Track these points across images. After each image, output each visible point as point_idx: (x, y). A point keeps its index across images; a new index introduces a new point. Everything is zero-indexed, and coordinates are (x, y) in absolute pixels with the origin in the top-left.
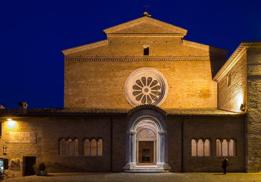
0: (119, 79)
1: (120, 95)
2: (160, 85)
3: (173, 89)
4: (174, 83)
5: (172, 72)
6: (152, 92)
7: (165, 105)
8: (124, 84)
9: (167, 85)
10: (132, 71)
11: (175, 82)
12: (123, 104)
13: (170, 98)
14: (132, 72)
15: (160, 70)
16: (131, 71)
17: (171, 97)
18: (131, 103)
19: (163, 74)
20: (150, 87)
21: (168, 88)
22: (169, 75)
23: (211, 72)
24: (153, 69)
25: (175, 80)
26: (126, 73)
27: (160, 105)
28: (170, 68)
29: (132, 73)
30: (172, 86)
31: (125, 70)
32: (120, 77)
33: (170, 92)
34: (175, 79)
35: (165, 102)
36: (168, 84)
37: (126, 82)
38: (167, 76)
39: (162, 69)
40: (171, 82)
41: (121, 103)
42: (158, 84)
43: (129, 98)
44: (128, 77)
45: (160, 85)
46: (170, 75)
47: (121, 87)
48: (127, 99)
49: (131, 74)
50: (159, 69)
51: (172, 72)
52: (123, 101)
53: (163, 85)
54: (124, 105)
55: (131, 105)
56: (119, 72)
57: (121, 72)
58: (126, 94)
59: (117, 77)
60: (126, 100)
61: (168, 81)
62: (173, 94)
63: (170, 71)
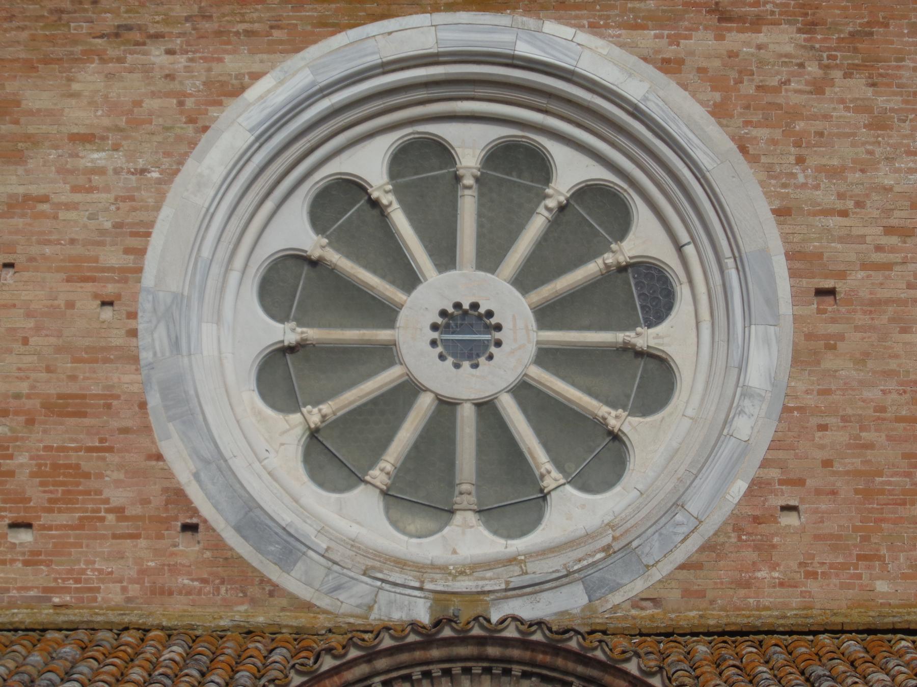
0: (63, 171)
1: (67, 407)
2: (599, 173)
3: (861, 318)
4: (874, 233)
5: (837, 74)
6: (547, 356)
7: (750, 555)
8: (141, 252)
9: (780, 266)
10: (256, 68)
11: (889, 230)
12: (106, 547)
13: (820, 455)
14: (256, 76)
15: (671, 52)
16: (233, 64)
17: (838, 437)
18: (238, 529)
19: (719, 112)
20: (410, 280)
21: (786, 308)
22: (800, 126)
23: (256, 389)
24: (567, 31)
25: (888, 189)
26: (168, 95)
27: (680, 556)
28: (810, 27)
29: (251, 94)
30: (855, 282)
31: (157, 55)
32: (87, 139)
33: (829, 362)
34: (885, 176)
35: (757, 520)
36: (789, 256)
37: (166, 212)
38: (777, 134)
39: (702, 44)
40: (820, 221)
41: (80, 526)
42: (370, 163)
43: (216, 463)
44: (193, 144)
45: (599, 173)
46: (819, 125)
47: (89, 287)
48: (183, 470)
49: (233, 107)
50: (648, 39)
51: (837, 74)
52: (118, 496)
53: (177, 338)
54: (121, 556)
55: (233, 560)
56: (70, 80)
57: (89, 79)
58: (154, 400)
59: (34, 141)
60: (154, 490)
61: (781, 213)
62: (873, 394)
63: (812, 68)
